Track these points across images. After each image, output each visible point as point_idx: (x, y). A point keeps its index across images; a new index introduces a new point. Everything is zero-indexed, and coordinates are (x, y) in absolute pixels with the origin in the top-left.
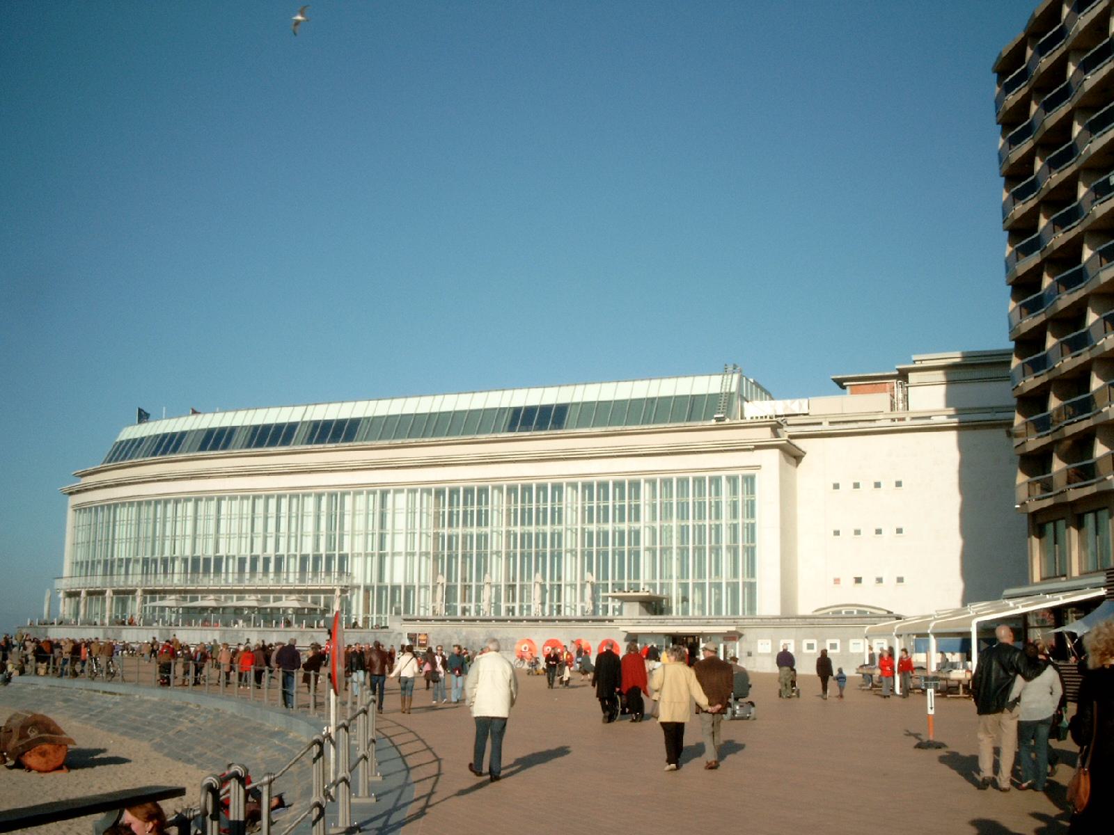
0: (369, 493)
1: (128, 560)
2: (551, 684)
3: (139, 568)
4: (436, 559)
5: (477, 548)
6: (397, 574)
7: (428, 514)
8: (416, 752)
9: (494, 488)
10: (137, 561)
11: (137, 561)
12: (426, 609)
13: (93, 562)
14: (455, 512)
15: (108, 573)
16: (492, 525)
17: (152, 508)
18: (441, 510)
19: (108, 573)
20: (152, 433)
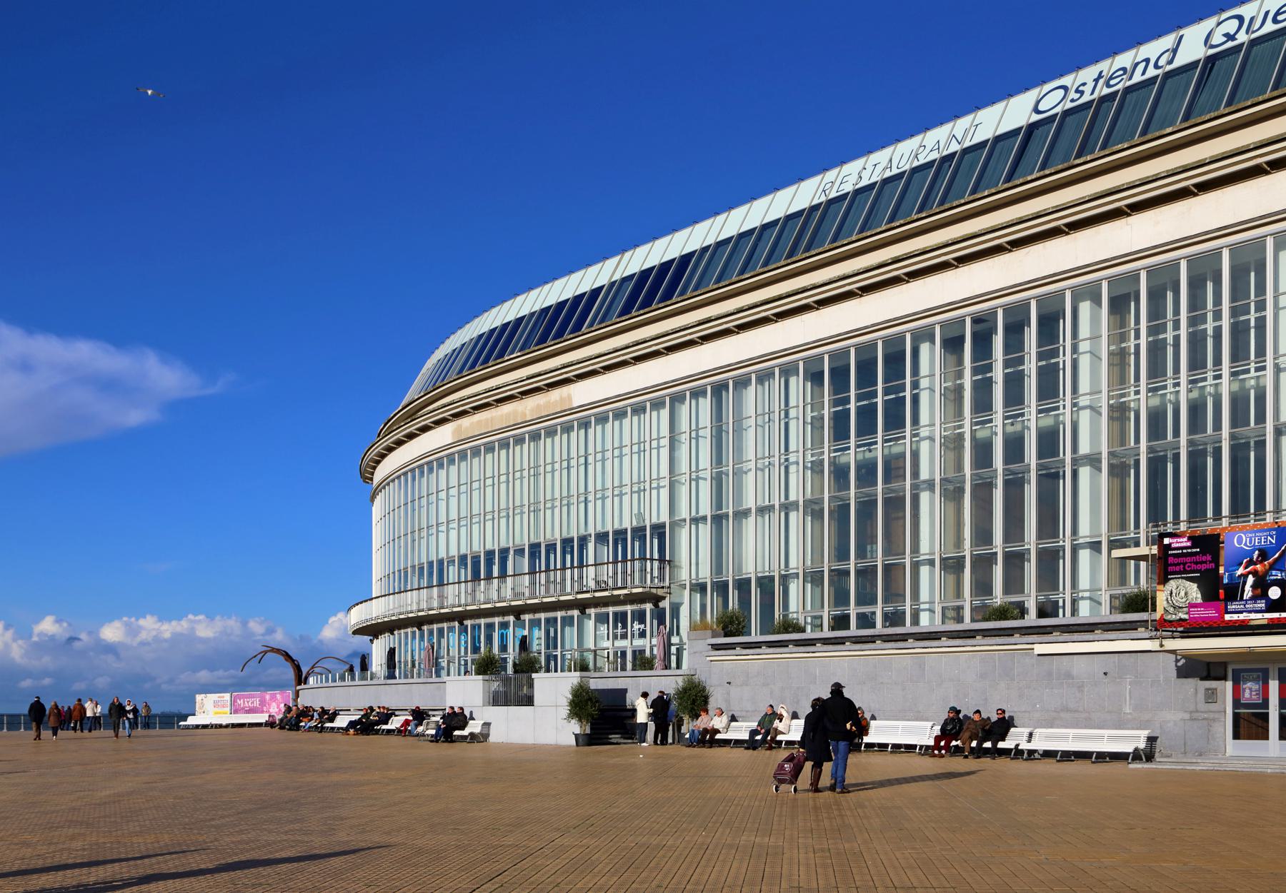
0: (760, 380)
1: (504, 552)
2: (117, 736)
3: (606, 553)
4: (1119, 471)
5: (1234, 424)
6: (755, 553)
7: (1095, 355)
8: (369, 848)
9: (1078, 296)
10: (451, 562)
11: (451, 562)
12: (1095, 602)
13: (441, 562)
14: (1210, 332)
15: (496, 573)
16: (916, 421)
17: (665, 413)
18: (1210, 326)
19: (496, 573)
20: (537, 308)
